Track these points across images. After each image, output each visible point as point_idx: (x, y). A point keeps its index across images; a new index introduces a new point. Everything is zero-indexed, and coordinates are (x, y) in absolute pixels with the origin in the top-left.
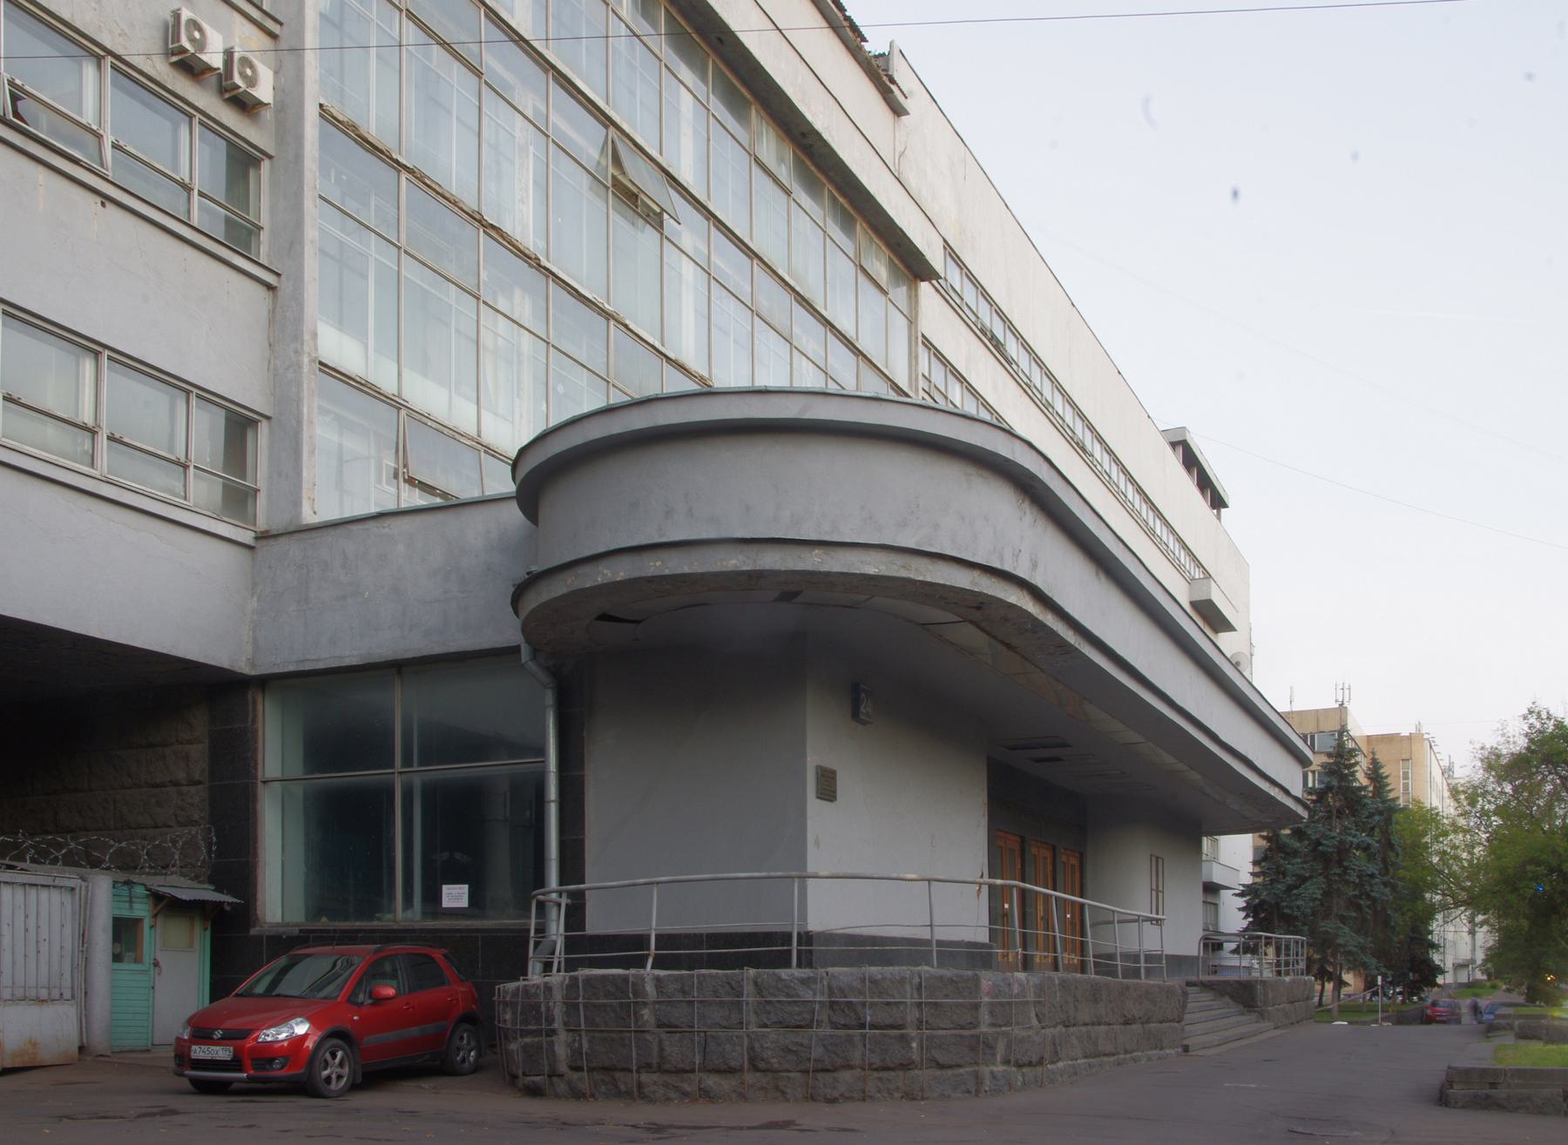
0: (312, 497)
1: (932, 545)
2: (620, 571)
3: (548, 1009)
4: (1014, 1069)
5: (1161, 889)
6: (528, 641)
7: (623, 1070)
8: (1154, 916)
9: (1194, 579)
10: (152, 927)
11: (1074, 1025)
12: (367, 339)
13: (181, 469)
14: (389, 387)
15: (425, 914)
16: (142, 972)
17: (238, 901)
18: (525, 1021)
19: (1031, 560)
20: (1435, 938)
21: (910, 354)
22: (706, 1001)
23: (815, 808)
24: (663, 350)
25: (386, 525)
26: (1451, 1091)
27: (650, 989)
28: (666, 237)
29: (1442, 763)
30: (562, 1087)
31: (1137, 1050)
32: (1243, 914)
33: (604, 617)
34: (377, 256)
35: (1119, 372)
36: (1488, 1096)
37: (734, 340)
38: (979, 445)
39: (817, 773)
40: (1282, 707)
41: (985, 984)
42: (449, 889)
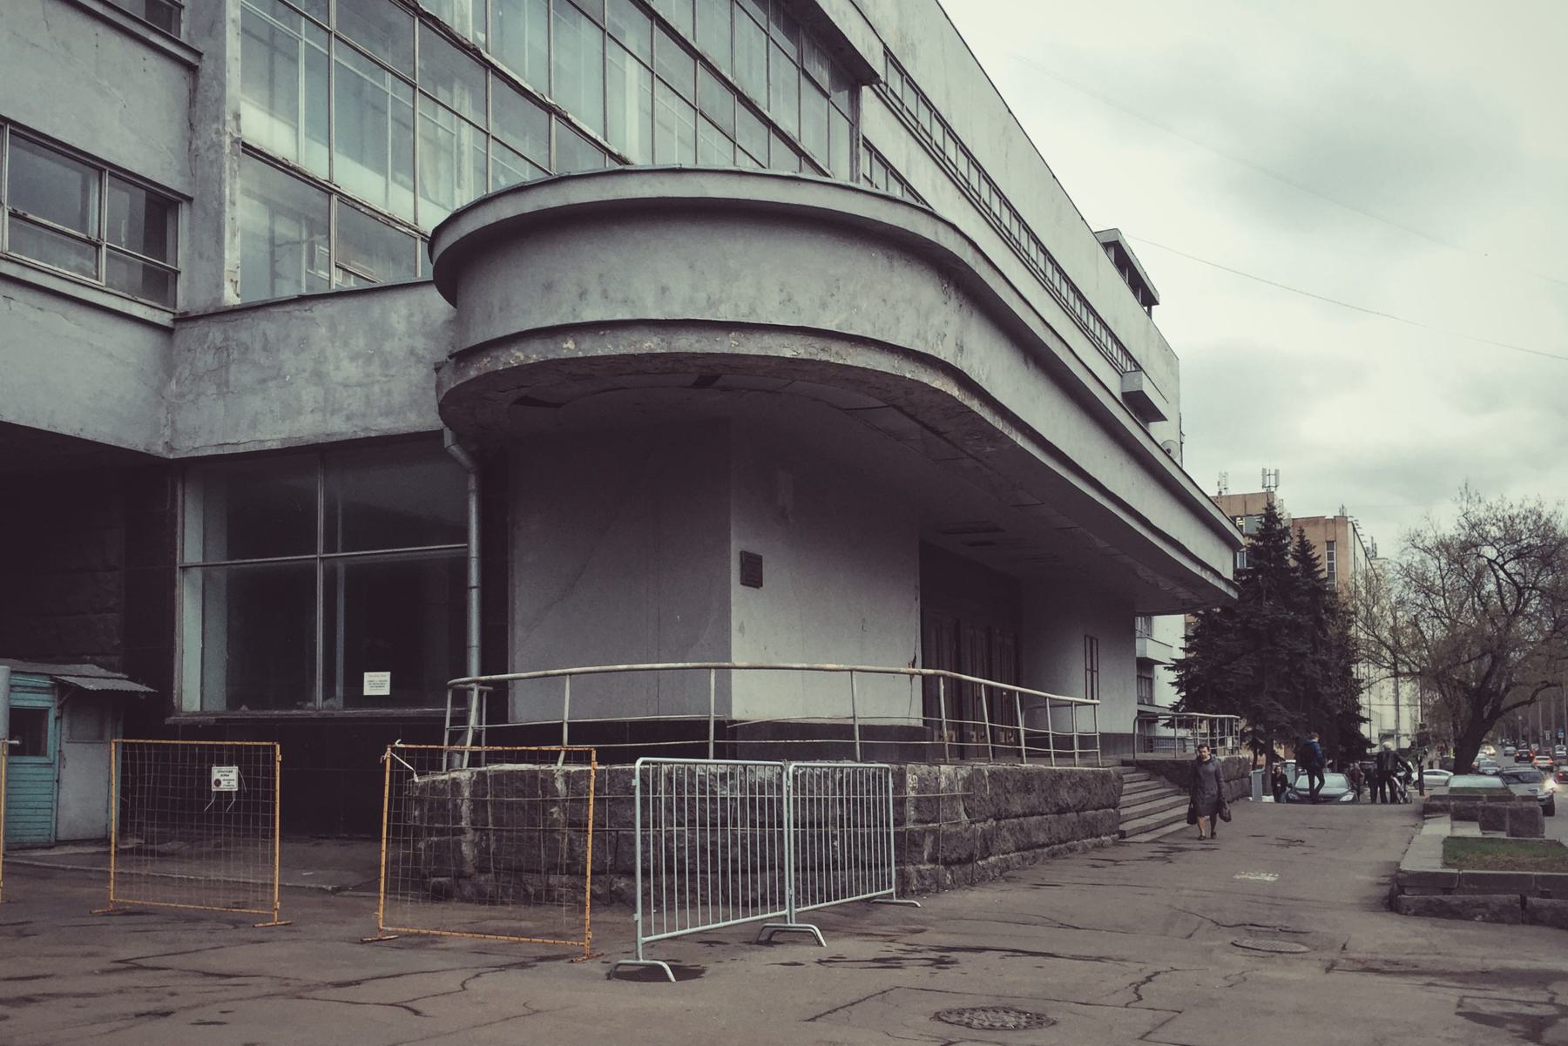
0: (235, 280)
1: (851, 328)
2: (532, 354)
3: (455, 805)
4: (942, 867)
5: (1095, 669)
6: (447, 423)
7: (531, 871)
8: (1089, 701)
9: (1125, 372)
10: (57, 718)
11: (1006, 817)
12: (297, 122)
13: (94, 248)
14: (321, 173)
15: (347, 704)
16: (50, 765)
17: (152, 690)
18: (431, 819)
19: (957, 345)
20: (1364, 713)
21: (851, 153)
22: (617, 798)
23: (738, 592)
24: (606, 145)
25: (307, 308)
26: (1403, 896)
27: (560, 785)
28: (739, 146)
29: (1365, 545)
30: (468, 890)
31: (1072, 839)
32: (1176, 689)
33: (525, 401)
34: (308, 41)
35: (1054, 177)
36: (1441, 903)
37: (679, 137)
38: (902, 226)
39: (741, 560)
40: (1212, 492)
41: (911, 780)
42: (370, 676)
